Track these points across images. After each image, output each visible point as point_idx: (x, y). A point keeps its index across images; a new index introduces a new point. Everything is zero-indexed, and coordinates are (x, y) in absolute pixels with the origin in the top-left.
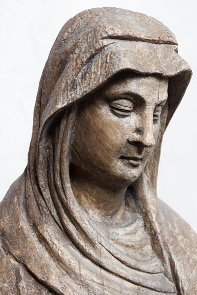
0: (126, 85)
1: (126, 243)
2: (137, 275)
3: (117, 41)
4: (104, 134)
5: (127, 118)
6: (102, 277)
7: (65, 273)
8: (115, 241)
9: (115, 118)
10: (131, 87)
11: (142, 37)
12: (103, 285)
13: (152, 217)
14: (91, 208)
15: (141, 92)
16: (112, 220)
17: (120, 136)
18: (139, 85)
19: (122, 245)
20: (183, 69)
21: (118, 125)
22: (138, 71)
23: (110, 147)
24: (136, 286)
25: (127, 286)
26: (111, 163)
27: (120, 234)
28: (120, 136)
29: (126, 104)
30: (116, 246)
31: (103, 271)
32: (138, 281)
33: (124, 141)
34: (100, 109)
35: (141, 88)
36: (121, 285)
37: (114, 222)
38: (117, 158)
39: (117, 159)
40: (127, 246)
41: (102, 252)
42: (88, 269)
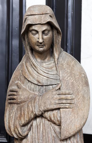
1: (46, 67)
6: (38, 76)
9: (33, 36)
11: (36, 14)
12: (38, 78)
17: (35, 40)
18: (35, 27)
21: (33, 37)
22: (53, 23)
23: (33, 43)
29: (34, 32)
30: (43, 68)
31: (48, 74)
33: (36, 42)
35: (36, 28)
36: (43, 78)
40: (46, 68)
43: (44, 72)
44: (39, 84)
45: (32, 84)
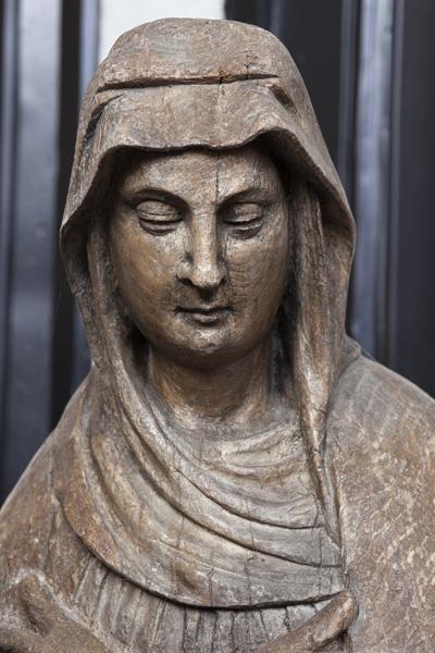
0: (142, 174)
1: (236, 469)
2: (252, 531)
3: (126, 92)
4: (135, 267)
5: (169, 235)
6: (180, 533)
7: (119, 523)
8: (212, 467)
9: (147, 238)
10: (151, 178)
11: (177, 76)
12: (177, 547)
13: (308, 419)
14: (178, 404)
15: (170, 185)
16: (226, 425)
17: (159, 270)
18: (166, 173)
19: (227, 473)
20: (260, 128)
21: (151, 248)
24: (249, 552)
25: (230, 551)
26: (162, 321)
27: (224, 452)
28: (159, 270)
29: (157, 211)
32: (250, 543)
33: (172, 280)
34: (124, 221)
35: (170, 178)
36: (214, 550)
37: (229, 430)
38: (169, 311)
39: (173, 314)
41: (181, 486)
42: (157, 518)
43: (225, 507)
44: (187, 598)
45: (130, 596)
